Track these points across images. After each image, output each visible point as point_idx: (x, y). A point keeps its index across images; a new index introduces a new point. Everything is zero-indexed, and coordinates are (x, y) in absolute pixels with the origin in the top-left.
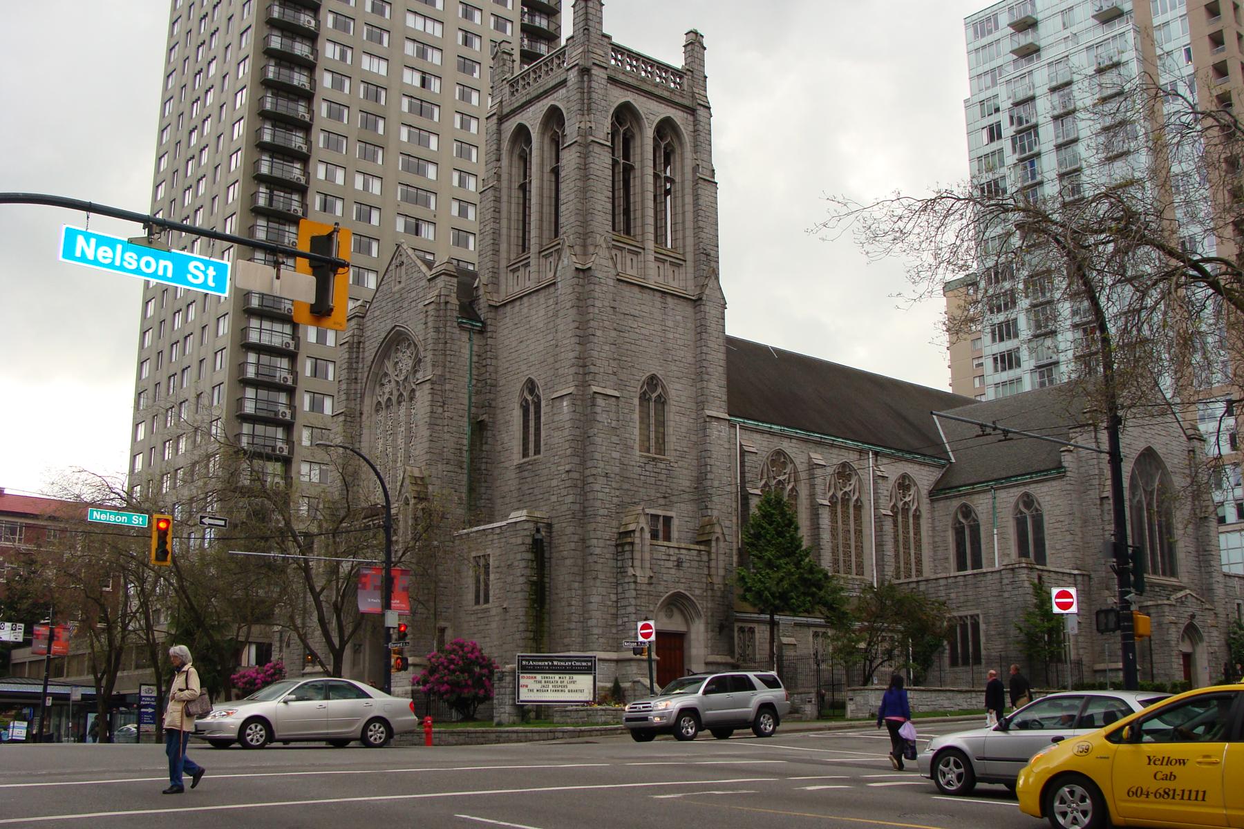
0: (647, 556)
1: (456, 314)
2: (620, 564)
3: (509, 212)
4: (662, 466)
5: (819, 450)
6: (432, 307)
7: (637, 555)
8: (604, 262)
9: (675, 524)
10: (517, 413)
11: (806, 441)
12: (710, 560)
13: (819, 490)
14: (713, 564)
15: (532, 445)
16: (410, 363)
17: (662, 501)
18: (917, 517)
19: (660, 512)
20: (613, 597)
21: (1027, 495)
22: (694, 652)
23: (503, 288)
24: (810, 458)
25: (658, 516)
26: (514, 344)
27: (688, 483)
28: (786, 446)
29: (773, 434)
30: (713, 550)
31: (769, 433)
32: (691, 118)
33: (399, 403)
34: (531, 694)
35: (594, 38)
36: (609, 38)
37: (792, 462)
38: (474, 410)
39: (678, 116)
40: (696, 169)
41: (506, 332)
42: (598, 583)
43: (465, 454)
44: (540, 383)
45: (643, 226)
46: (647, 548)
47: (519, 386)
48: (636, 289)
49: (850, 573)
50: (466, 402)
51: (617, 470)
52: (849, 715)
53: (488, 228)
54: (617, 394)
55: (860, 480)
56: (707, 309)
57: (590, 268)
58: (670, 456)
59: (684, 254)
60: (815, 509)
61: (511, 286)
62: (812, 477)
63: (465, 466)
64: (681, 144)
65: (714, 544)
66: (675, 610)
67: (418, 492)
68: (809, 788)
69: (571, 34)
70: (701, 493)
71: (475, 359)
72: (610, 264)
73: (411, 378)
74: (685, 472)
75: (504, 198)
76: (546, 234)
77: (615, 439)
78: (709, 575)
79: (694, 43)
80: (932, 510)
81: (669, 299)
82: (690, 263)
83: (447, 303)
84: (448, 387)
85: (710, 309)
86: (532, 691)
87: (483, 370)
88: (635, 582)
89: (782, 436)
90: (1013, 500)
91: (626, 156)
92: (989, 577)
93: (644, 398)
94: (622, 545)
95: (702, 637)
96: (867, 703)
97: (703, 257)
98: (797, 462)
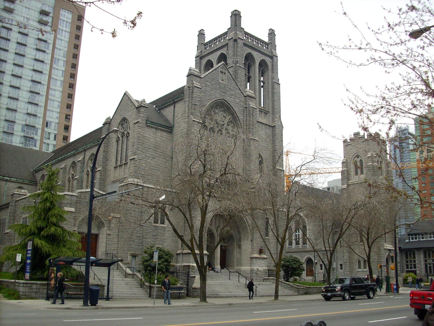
32: (271, 60)
36: (243, 29)
49: (157, 223)
57: (275, 126)
59: (268, 110)
69: (230, 27)
79: (272, 34)
91: (249, 73)
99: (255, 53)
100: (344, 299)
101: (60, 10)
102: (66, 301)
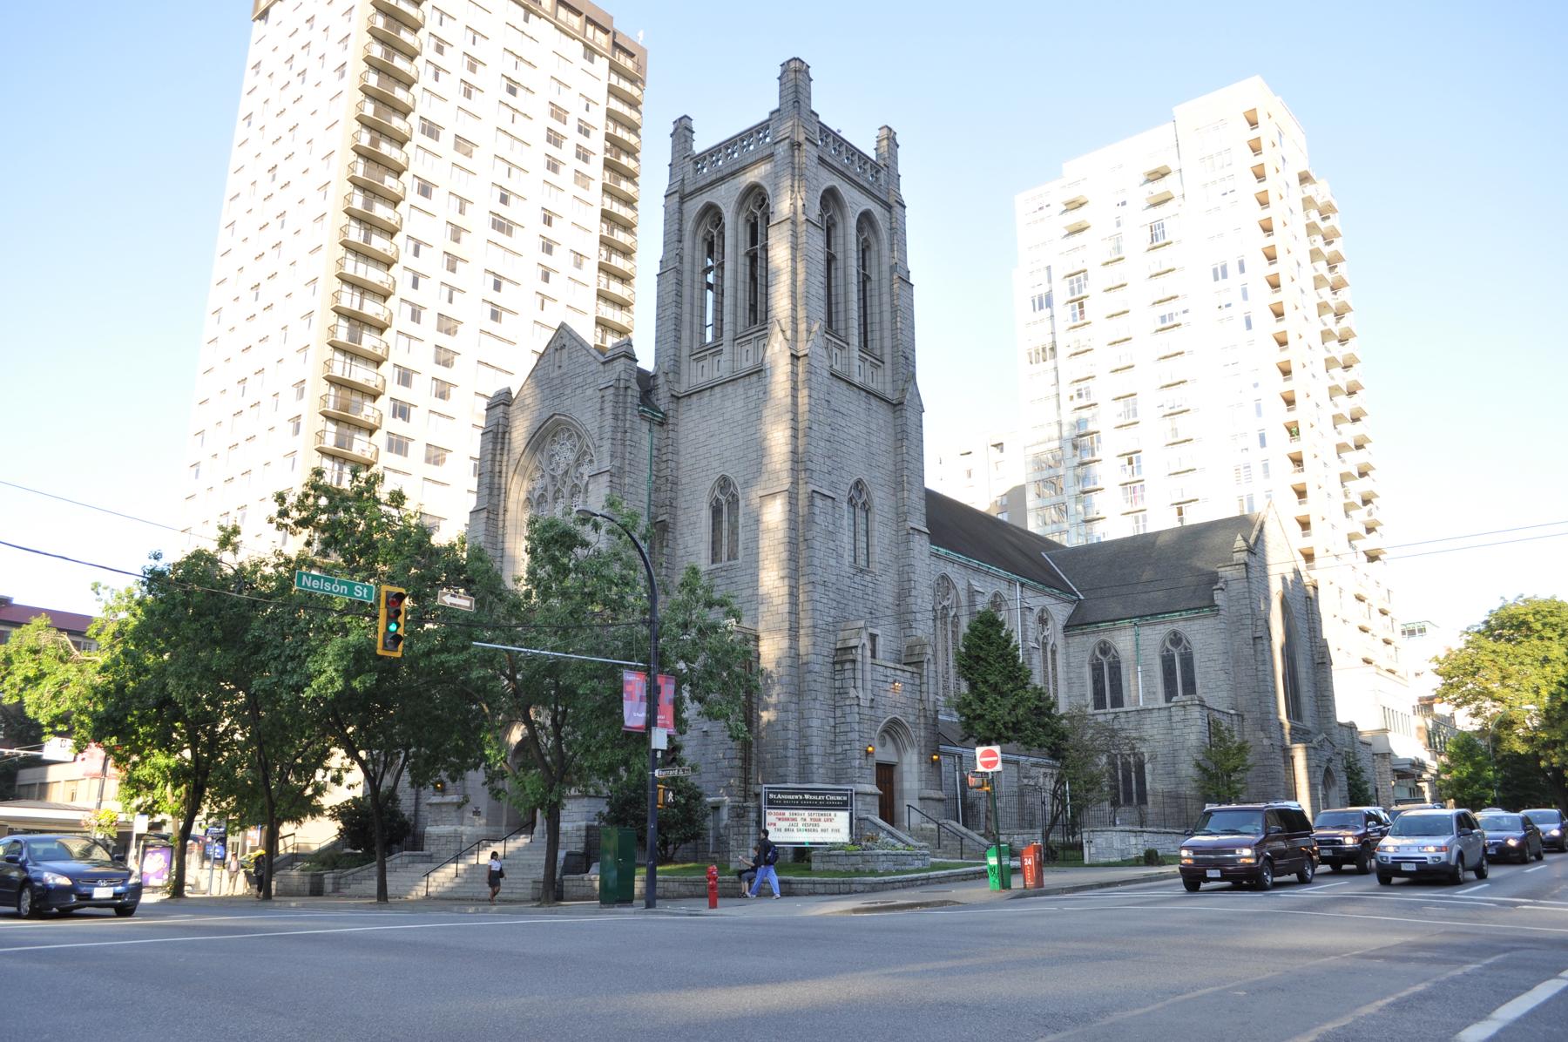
1: (637, 401)
2: (838, 684)
3: (692, 297)
6: (611, 390)
10: (705, 515)
11: (966, 566)
15: (725, 549)
16: (572, 457)
18: (1054, 652)
20: (832, 721)
21: (1175, 633)
22: (907, 785)
23: (684, 378)
24: (970, 585)
26: (702, 439)
28: (950, 570)
33: (555, 499)
35: (804, 114)
40: (893, 268)
41: (691, 425)
44: (738, 481)
45: (846, 320)
46: (868, 667)
47: (709, 484)
50: (646, 499)
52: (1086, 861)
53: (668, 313)
61: (695, 375)
64: (878, 241)
69: (776, 106)
71: (655, 453)
72: (825, 354)
73: (572, 471)
75: (687, 282)
76: (740, 321)
79: (890, 139)
80: (1067, 645)
82: (888, 365)
84: (627, 480)
85: (909, 414)
87: (663, 466)
90: (1159, 638)
92: (1155, 714)
94: (842, 663)
95: (915, 769)
96: (1111, 846)
97: (902, 360)
98: (959, 587)
99: (845, 190)
100: (742, 895)
101: (263, 823)
102: (719, 902)
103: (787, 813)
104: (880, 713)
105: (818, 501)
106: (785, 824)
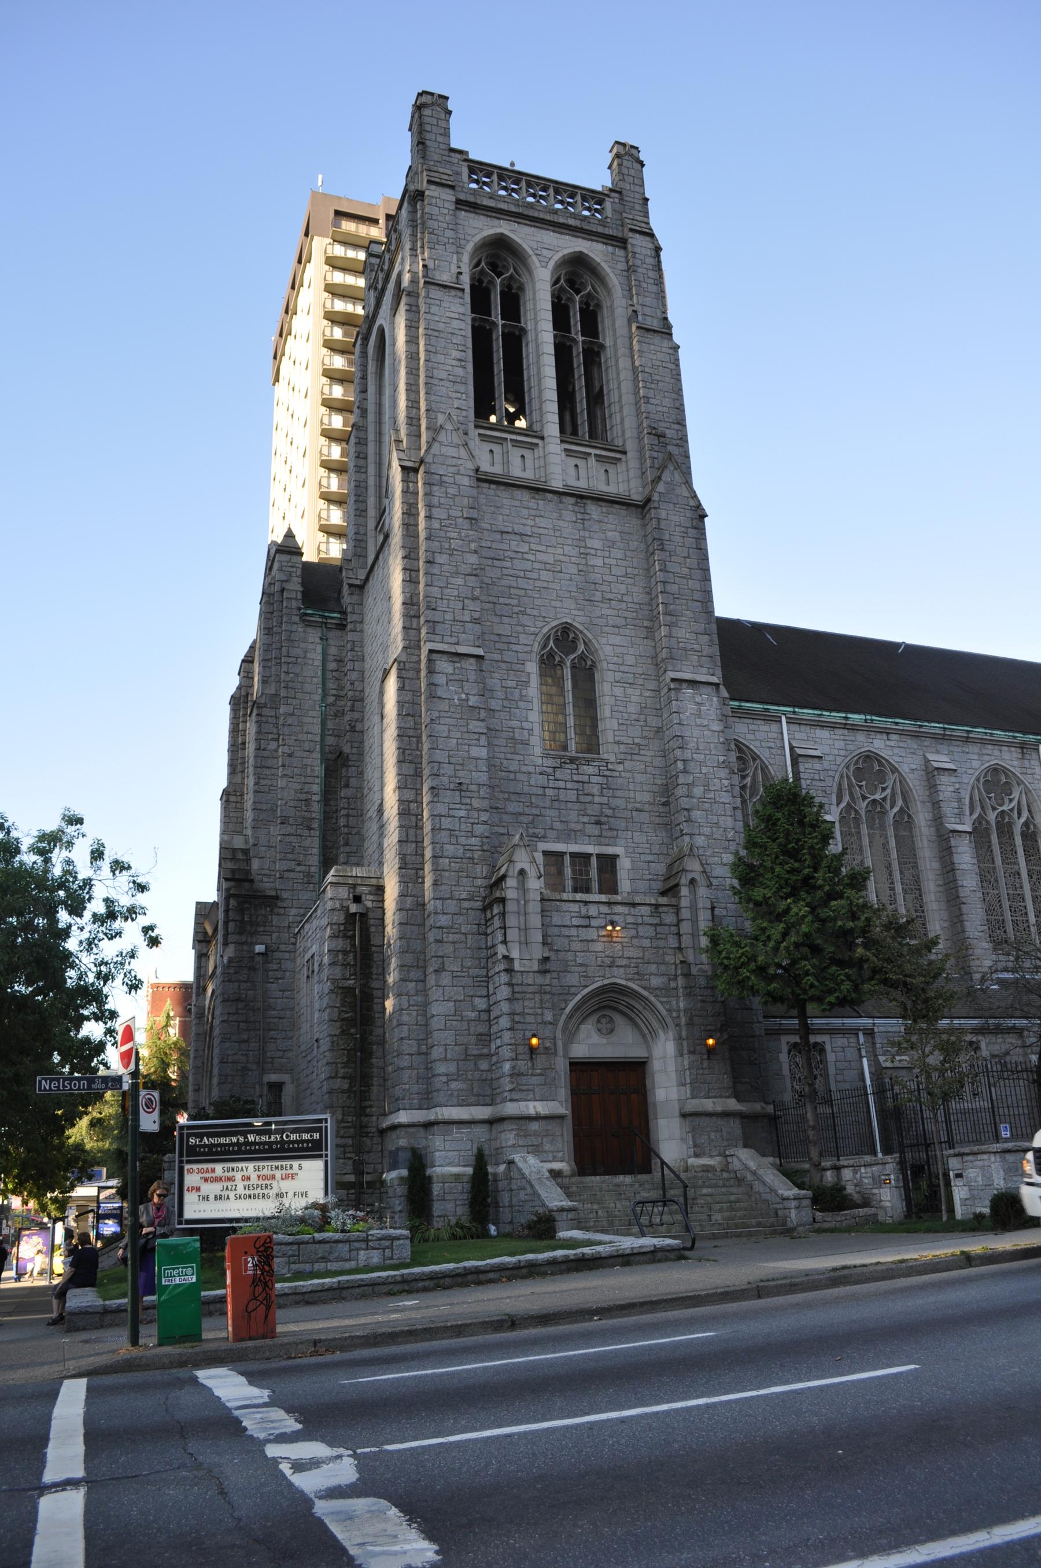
0: (535, 921)
4: (590, 770)
5: (944, 748)
7: (511, 921)
8: (452, 452)
9: (624, 865)
11: (916, 736)
12: (679, 921)
13: (948, 809)
14: (686, 927)
17: (594, 830)
19: (590, 849)
24: (927, 761)
25: (587, 856)
27: (647, 797)
28: (879, 745)
29: (854, 728)
30: (685, 902)
31: (844, 727)
32: (619, 252)
34: (204, 1205)
37: (894, 770)
38: (330, 740)
39: (596, 251)
42: (446, 979)
43: (316, 807)
48: (524, 496)
50: (317, 729)
51: (483, 778)
54: (480, 652)
55: (1027, 792)
56: (663, 514)
58: (608, 752)
60: (944, 840)
62: (932, 787)
63: (316, 825)
64: (609, 292)
65: (684, 891)
66: (618, 1019)
67: (233, 871)
68: (912, 1367)
70: (669, 807)
71: (332, 666)
74: (639, 778)
77: (476, 726)
78: (680, 949)
79: (627, 158)
81: (593, 509)
83: (283, 590)
84: (283, 709)
86: (206, 1198)
88: (509, 971)
89: (869, 729)
93: (548, 663)
95: (672, 1067)
98: (904, 769)
99: (522, 235)
103: (219, 1168)
104: (572, 979)
105: (444, 665)
106: (215, 1188)
